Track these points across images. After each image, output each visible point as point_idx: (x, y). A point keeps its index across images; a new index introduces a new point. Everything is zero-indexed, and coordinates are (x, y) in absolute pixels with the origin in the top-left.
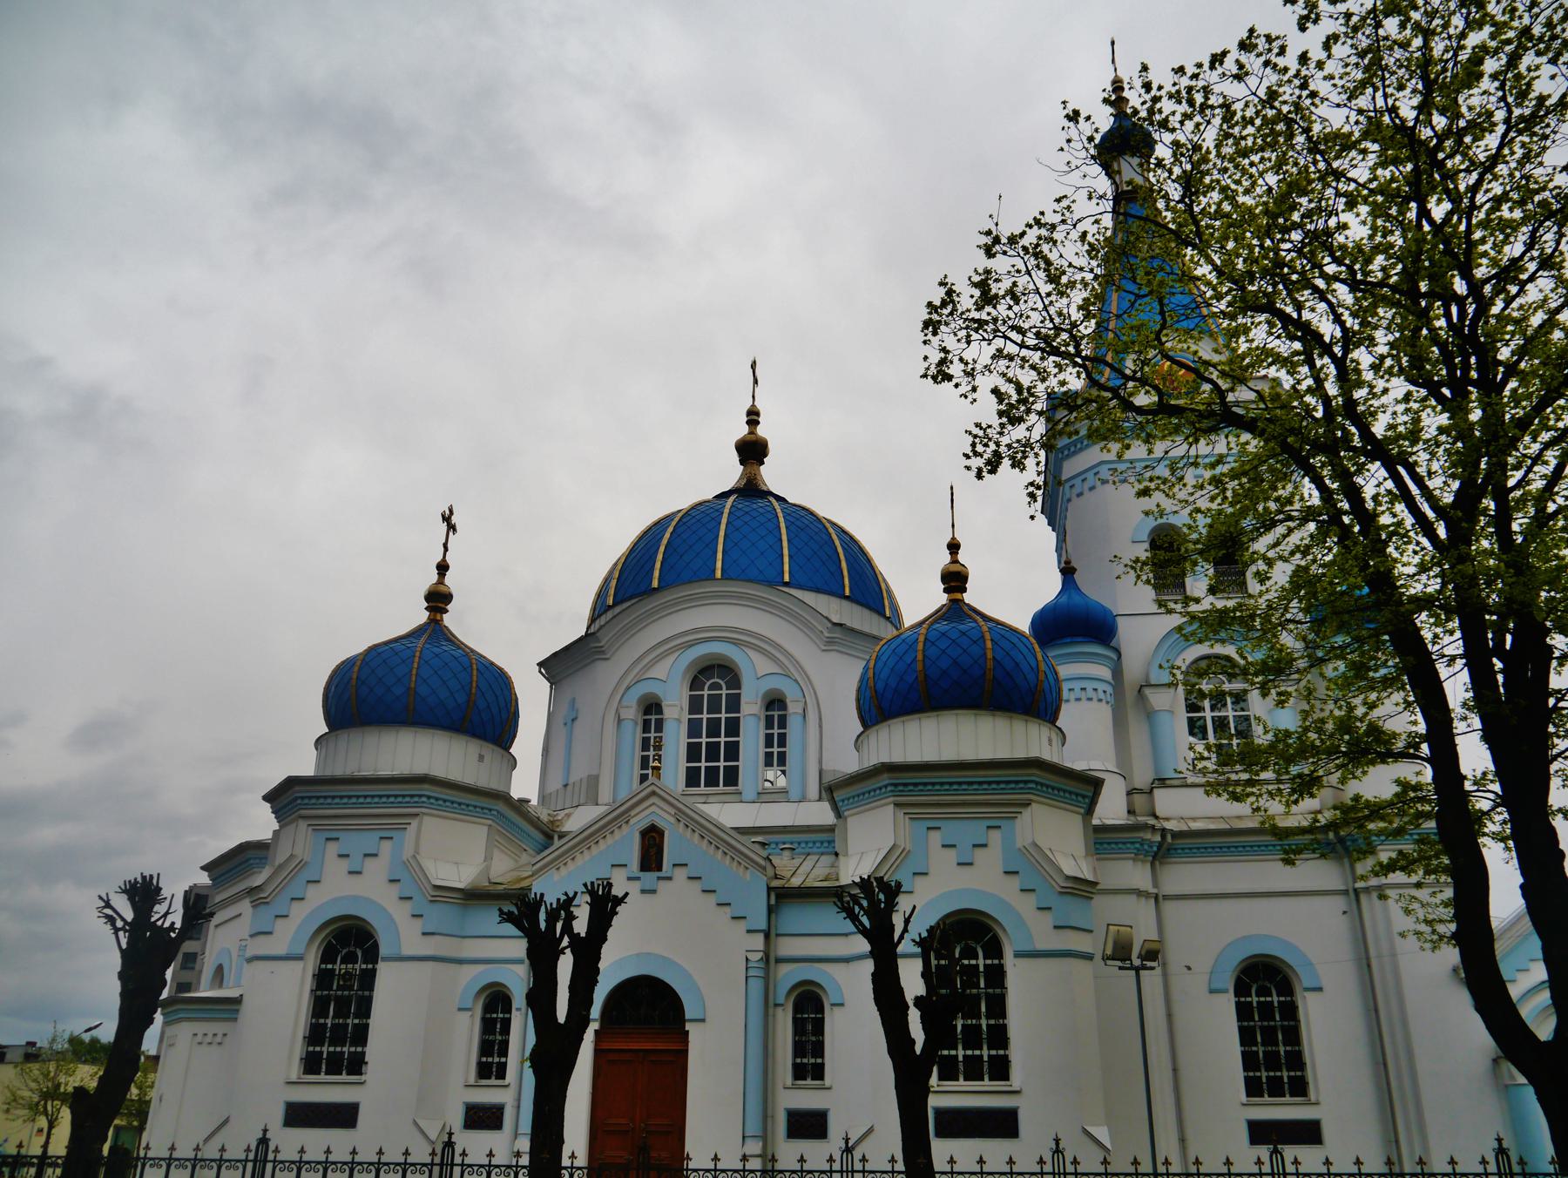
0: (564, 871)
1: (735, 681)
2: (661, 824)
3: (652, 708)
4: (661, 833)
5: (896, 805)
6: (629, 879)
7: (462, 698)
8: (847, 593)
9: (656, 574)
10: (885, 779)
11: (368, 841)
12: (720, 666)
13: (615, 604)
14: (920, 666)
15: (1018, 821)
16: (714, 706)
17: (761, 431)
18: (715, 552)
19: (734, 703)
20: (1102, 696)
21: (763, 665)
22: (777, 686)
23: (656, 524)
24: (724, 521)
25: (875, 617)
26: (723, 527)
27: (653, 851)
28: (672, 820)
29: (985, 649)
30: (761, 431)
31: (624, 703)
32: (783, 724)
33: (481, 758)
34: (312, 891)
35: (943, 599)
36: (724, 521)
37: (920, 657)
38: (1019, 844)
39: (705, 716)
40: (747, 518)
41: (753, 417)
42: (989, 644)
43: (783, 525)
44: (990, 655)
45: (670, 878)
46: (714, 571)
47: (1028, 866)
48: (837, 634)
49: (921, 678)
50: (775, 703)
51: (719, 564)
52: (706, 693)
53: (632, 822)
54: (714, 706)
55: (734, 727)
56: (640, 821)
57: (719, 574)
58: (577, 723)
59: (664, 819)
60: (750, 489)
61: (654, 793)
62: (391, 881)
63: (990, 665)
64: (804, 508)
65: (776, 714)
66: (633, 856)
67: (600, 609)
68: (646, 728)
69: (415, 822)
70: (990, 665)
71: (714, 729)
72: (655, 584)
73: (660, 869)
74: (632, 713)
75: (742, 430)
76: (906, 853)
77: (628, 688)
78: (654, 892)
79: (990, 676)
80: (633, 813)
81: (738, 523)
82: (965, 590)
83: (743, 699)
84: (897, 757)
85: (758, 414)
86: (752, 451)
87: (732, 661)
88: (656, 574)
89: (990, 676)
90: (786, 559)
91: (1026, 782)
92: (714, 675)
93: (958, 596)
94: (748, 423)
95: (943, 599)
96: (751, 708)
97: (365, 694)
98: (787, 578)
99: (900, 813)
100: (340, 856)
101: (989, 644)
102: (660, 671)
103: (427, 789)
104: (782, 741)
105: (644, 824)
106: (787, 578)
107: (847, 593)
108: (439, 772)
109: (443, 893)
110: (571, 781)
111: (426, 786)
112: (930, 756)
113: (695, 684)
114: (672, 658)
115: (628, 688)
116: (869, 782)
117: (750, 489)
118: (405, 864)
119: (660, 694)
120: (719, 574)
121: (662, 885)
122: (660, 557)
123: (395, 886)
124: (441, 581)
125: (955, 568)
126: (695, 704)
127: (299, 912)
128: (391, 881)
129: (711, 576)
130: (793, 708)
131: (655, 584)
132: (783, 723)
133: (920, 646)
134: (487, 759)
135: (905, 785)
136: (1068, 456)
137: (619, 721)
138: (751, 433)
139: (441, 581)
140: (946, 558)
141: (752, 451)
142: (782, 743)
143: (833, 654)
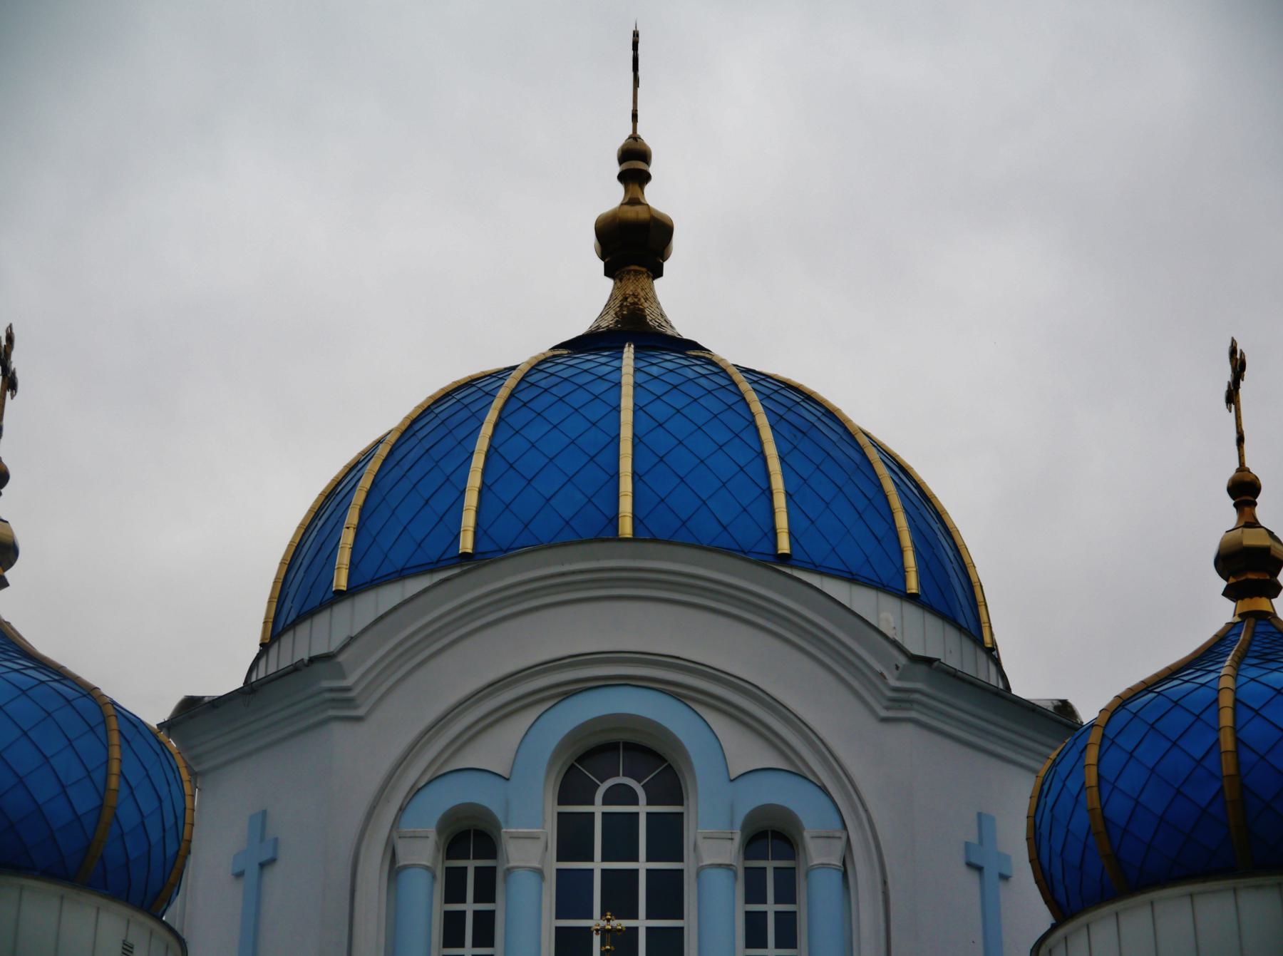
8: (913, 585)
12: (631, 747)
13: (354, 590)
14: (1228, 767)
16: (620, 838)
17: (656, 197)
18: (616, 476)
19: (668, 837)
21: (744, 752)
22: (792, 806)
23: (470, 383)
24: (627, 403)
26: (627, 416)
30: (656, 197)
31: (406, 828)
32: (787, 892)
35: (1226, 612)
36: (627, 403)
37: (1227, 743)
40: (579, 398)
41: (634, 164)
46: (614, 519)
50: (770, 838)
51: (626, 505)
52: (598, 809)
54: (620, 838)
57: (626, 528)
58: (274, 876)
60: (633, 328)
64: (796, 389)
65: (471, 865)
67: (301, 590)
68: (454, 890)
72: (467, 543)
74: (423, 852)
75: (612, 196)
77: (416, 791)
81: (659, 410)
83: (691, 833)
85: (644, 156)
86: (633, 244)
92: (622, 766)
93: (1262, 604)
94: (622, 177)
96: (712, 845)
98: (784, 546)
102: (494, 751)
106: (784, 546)
107: (913, 585)
113: (572, 787)
115: (416, 791)
120: (626, 528)
122: (475, 480)
126: (573, 839)
130: (818, 853)
131: (467, 543)
132: (487, 886)
133: (1226, 718)
137: (394, 870)
138: (633, 201)
140: (612, 196)
141: (633, 244)
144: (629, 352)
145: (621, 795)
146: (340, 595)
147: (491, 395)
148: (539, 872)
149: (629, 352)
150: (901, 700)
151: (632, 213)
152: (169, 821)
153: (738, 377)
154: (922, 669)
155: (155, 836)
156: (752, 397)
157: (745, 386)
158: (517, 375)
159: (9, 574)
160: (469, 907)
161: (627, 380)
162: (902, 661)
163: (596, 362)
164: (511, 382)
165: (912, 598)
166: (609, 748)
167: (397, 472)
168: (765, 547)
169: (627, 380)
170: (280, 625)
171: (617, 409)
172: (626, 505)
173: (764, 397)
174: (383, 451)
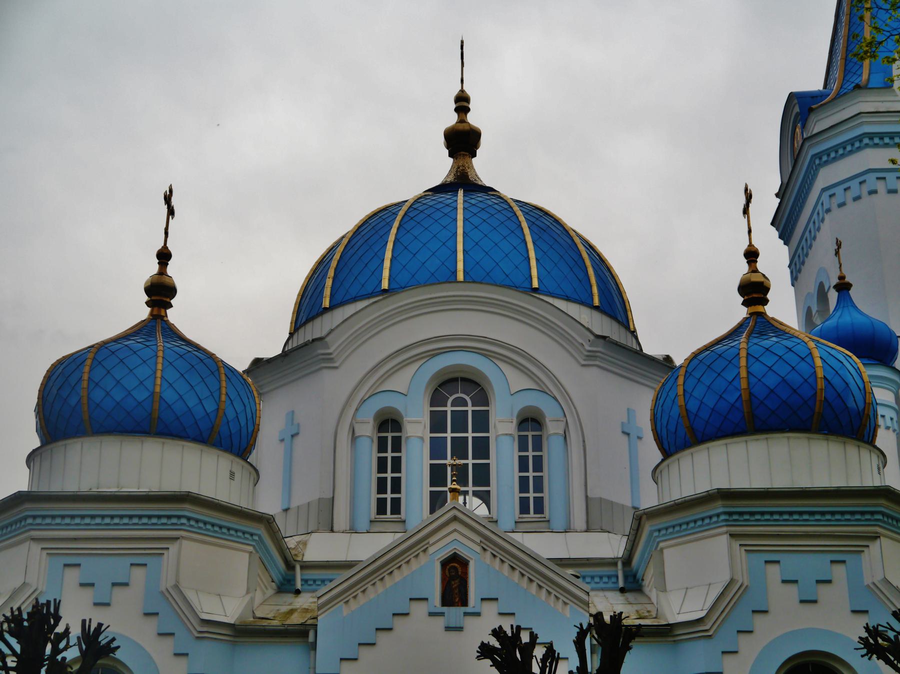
0: (354, 605)
1: (482, 396)
2: (464, 553)
3: (389, 424)
4: (465, 564)
5: (732, 536)
6: (431, 614)
7: (210, 407)
8: (596, 302)
9: (386, 273)
10: (718, 507)
11: (118, 567)
12: (464, 380)
14: (744, 384)
15: (865, 556)
16: (460, 423)
17: (473, 119)
19: (482, 422)
20: (889, 423)
21: (518, 381)
25: (623, 330)
26: (460, 223)
27: (455, 584)
28: (478, 549)
29: (813, 367)
30: (473, 119)
31: (359, 418)
32: (538, 446)
33: (232, 475)
34: (759, 622)
35: (742, 312)
37: (744, 373)
38: (867, 581)
39: (449, 435)
40: (438, 215)
41: (462, 103)
42: (819, 362)
43: (525, 225)
44: (820, 374)
45: (478, 614)
46: (455, 273)
47: (169, 610)
48: (599, 348)
49: (745, 397)
50: (530, 421)
51: (460, 266)
52: (449, 409)
53: (431, 550)
54: (460, 423)
55: (482, 448)
56: (440, 549)
57: (460, 276)
58: (298, 440)
59: (469, 548)
60: (461, 181)
61: (455, 519)
62: (147, 614)
63: (821, 384)
65: (390, 435)
66: (434, 589)
68: (382, 447)
69: (173, 548)
70: (821, 384)
71: (459, 448)
72: (385, 285)
73: (464, 602)
74: (367, 430)
75: (452, 119)
76: (744, 590)
77: (363, 401)
78: (460, 629)
79: (821, 396)
80: (432, 540)
81: (476, 220)
82: (765, 302)
84: (740, 482)
87: (485, 378)
88: (386, 273)
89: (821, 396)
90: (533, 263)
91: (872, 513)
93: (759, 308)
94: (456, 110)
95: (742, 312)
97: (81, 399)
98: (535, 284)
99: (736, 544)
100: (82, 585)
101: (819, 362)
102: (400, 382)
103: (188, 510)
104: (538, 464)
105: (445, 554)
106: (535, 284)
107: (596, 302)
108: (207, 491)
109: (211, 628)
110: (294, 504)
111: (187, 506)
112: (758, 482)
113: (437, 398)
114: (415, 367)
115: (363, 401)
116: (235, 519)
117: (461, 181)
118: (165, 595)
119: (401, 409)
120: (460, 276)
121: (469, 622)
123: (153, 621)
124: (162, 272)
125: (755, 278)
126: (437, 423)
127: (750, 648)
128: (147, 614)
129: (452, 277)
130: (553, 428)
131: (385, 285)
133: (743, 362)
134: (238, 476)
135: (741, 514)
136: (826, 163)
137: (354, 438)
138: (462, 121)
139: (162, 272)
140: (452, 119)
141: (462, 141)
142: (538, 466)
143: (595, 370)
144: (461, 193)
145: (462, 402)
146: (326, 310)
147: (395, 214)
148: (422, 438)
149: (461, 193)
150: (591, 356)
151: (461, 126)
152: (249, 416)
153: (513, 204)
154: (602, 341)
155: (243, 423)
156: (520, 214)
157: (516, 208)
158: (408, 205)
159: (172, 302)
160: (389, 455)
161: (460, 206)
162: (592, 337)
163: (445, 197)
164: (405, 208)
165: (596, 308)
166: (454, 380)
167: (352, 251)
168: (527, 285)
169: (460, 206)
170: (297, 325)
171: (455, 220)
172: (460, 266)
173: (525, 214)
174: (345, 241)
